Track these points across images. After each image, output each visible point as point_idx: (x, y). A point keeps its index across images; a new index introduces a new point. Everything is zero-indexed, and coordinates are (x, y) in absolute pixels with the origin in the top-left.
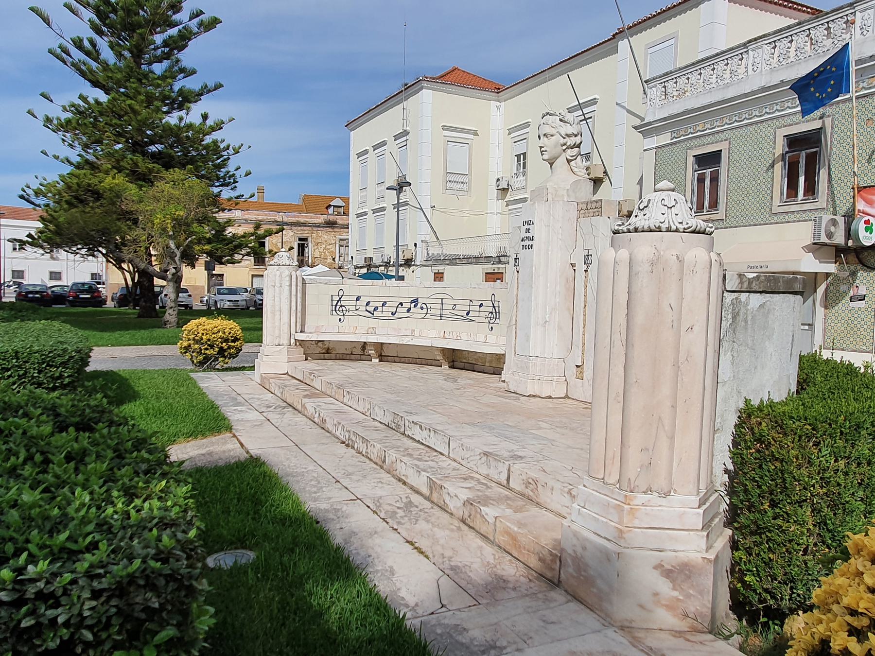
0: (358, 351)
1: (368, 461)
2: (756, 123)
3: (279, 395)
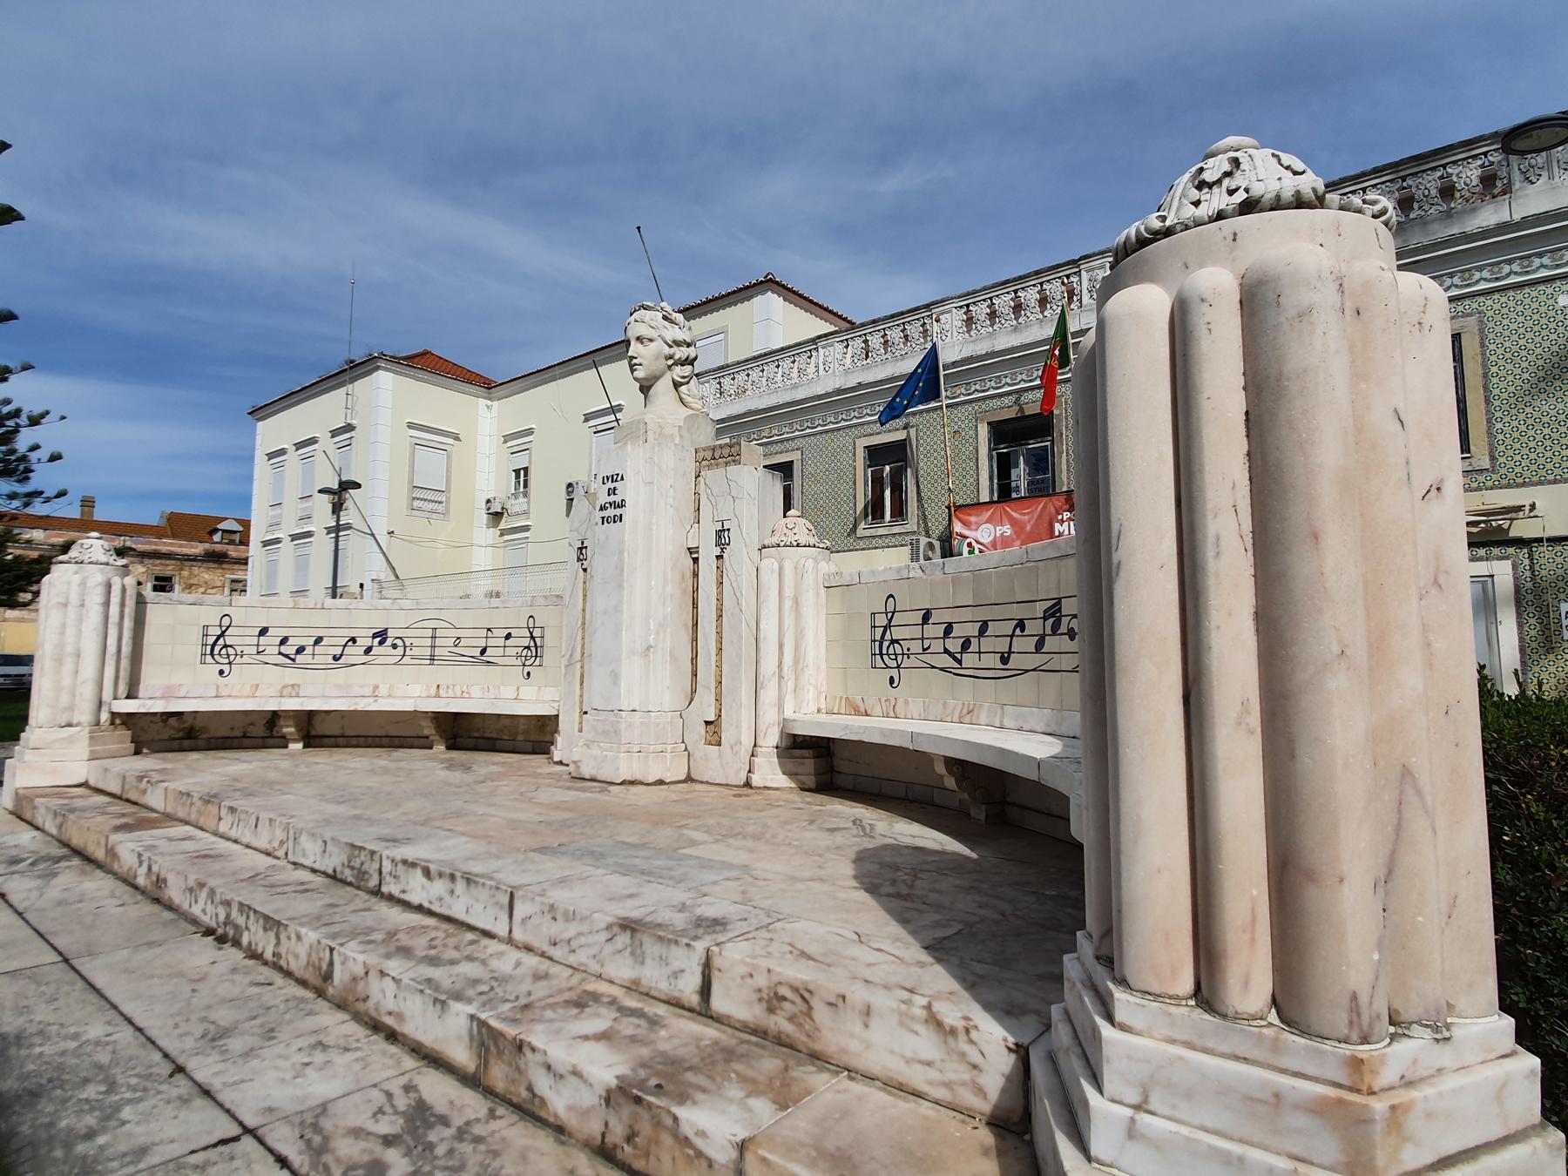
0: (259, 730)
1: (279, 980)
2: (832, 430)
3: (54, 831)
